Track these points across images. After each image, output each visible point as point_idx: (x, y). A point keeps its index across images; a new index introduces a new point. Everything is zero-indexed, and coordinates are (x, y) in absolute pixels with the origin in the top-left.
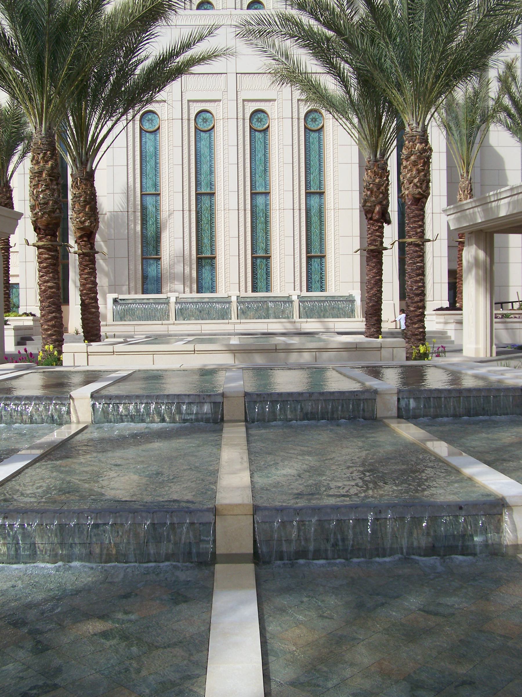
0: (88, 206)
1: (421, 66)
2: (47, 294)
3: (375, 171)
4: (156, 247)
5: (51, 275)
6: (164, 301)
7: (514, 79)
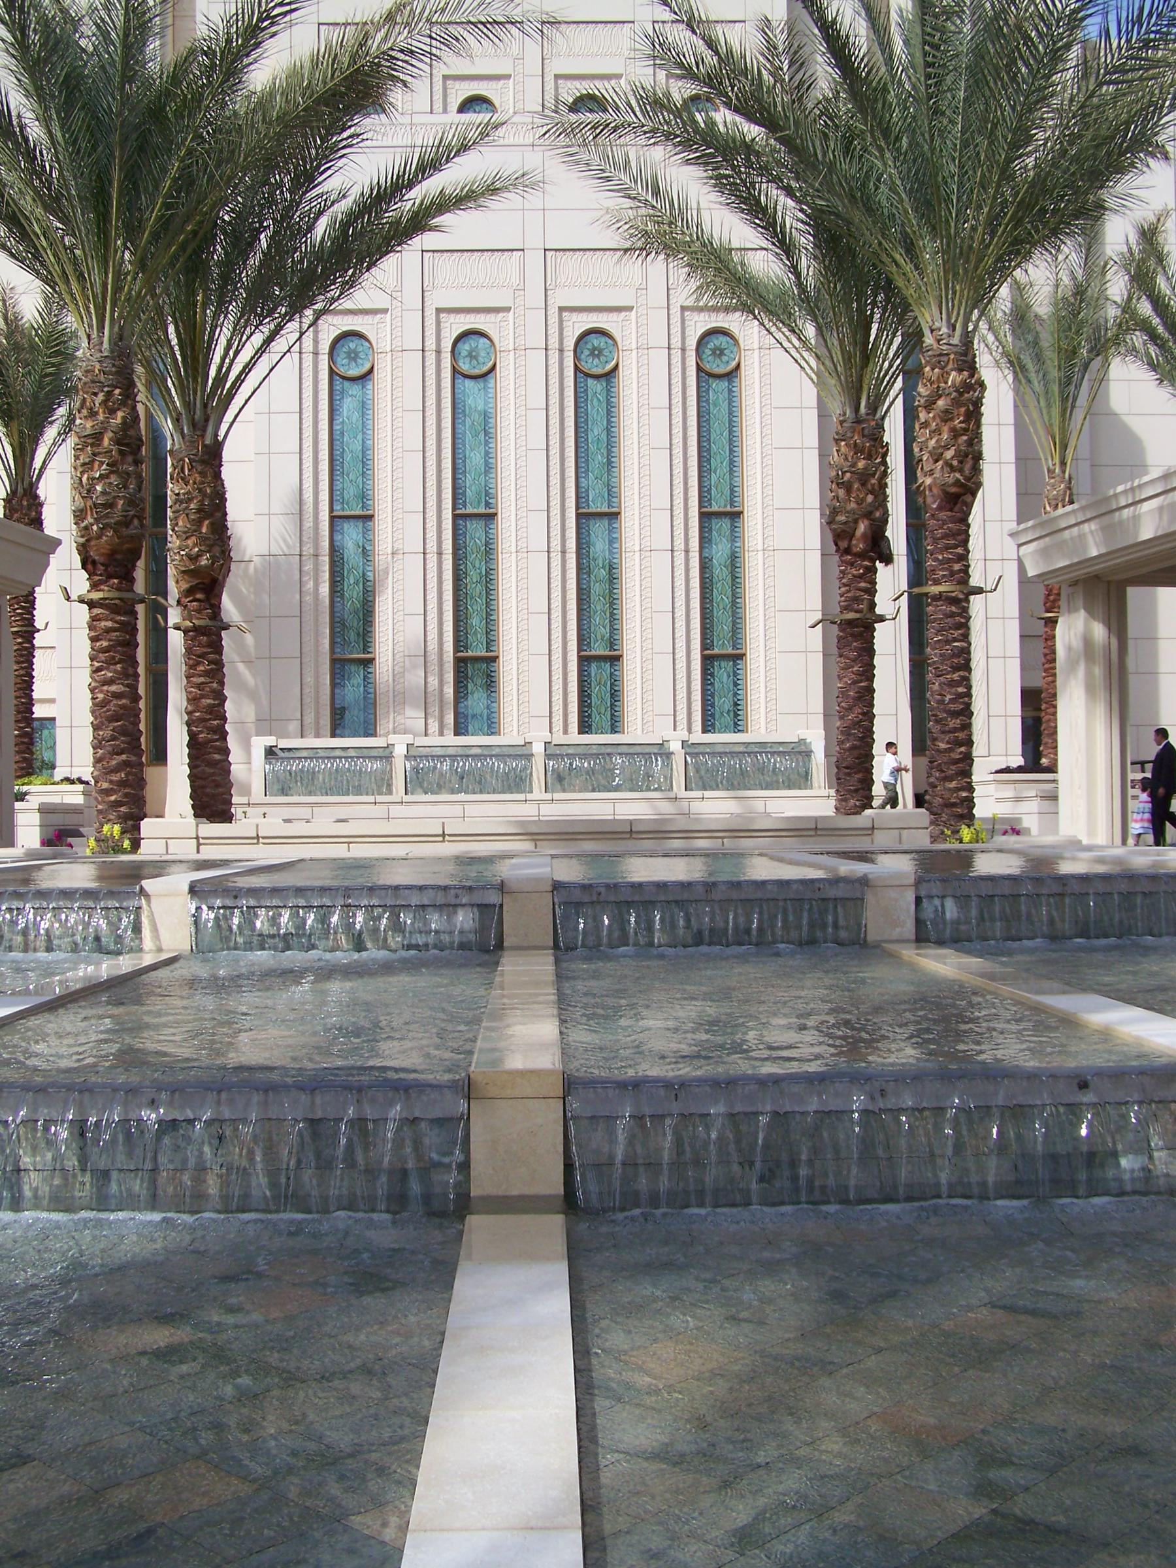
0: (207, 522)
1: (958, 201)
2: (108, 711)
3: (855, 444)
4: (364, 635)
5: (119, 667)
6: (380, 753)
7: (1161, 259)
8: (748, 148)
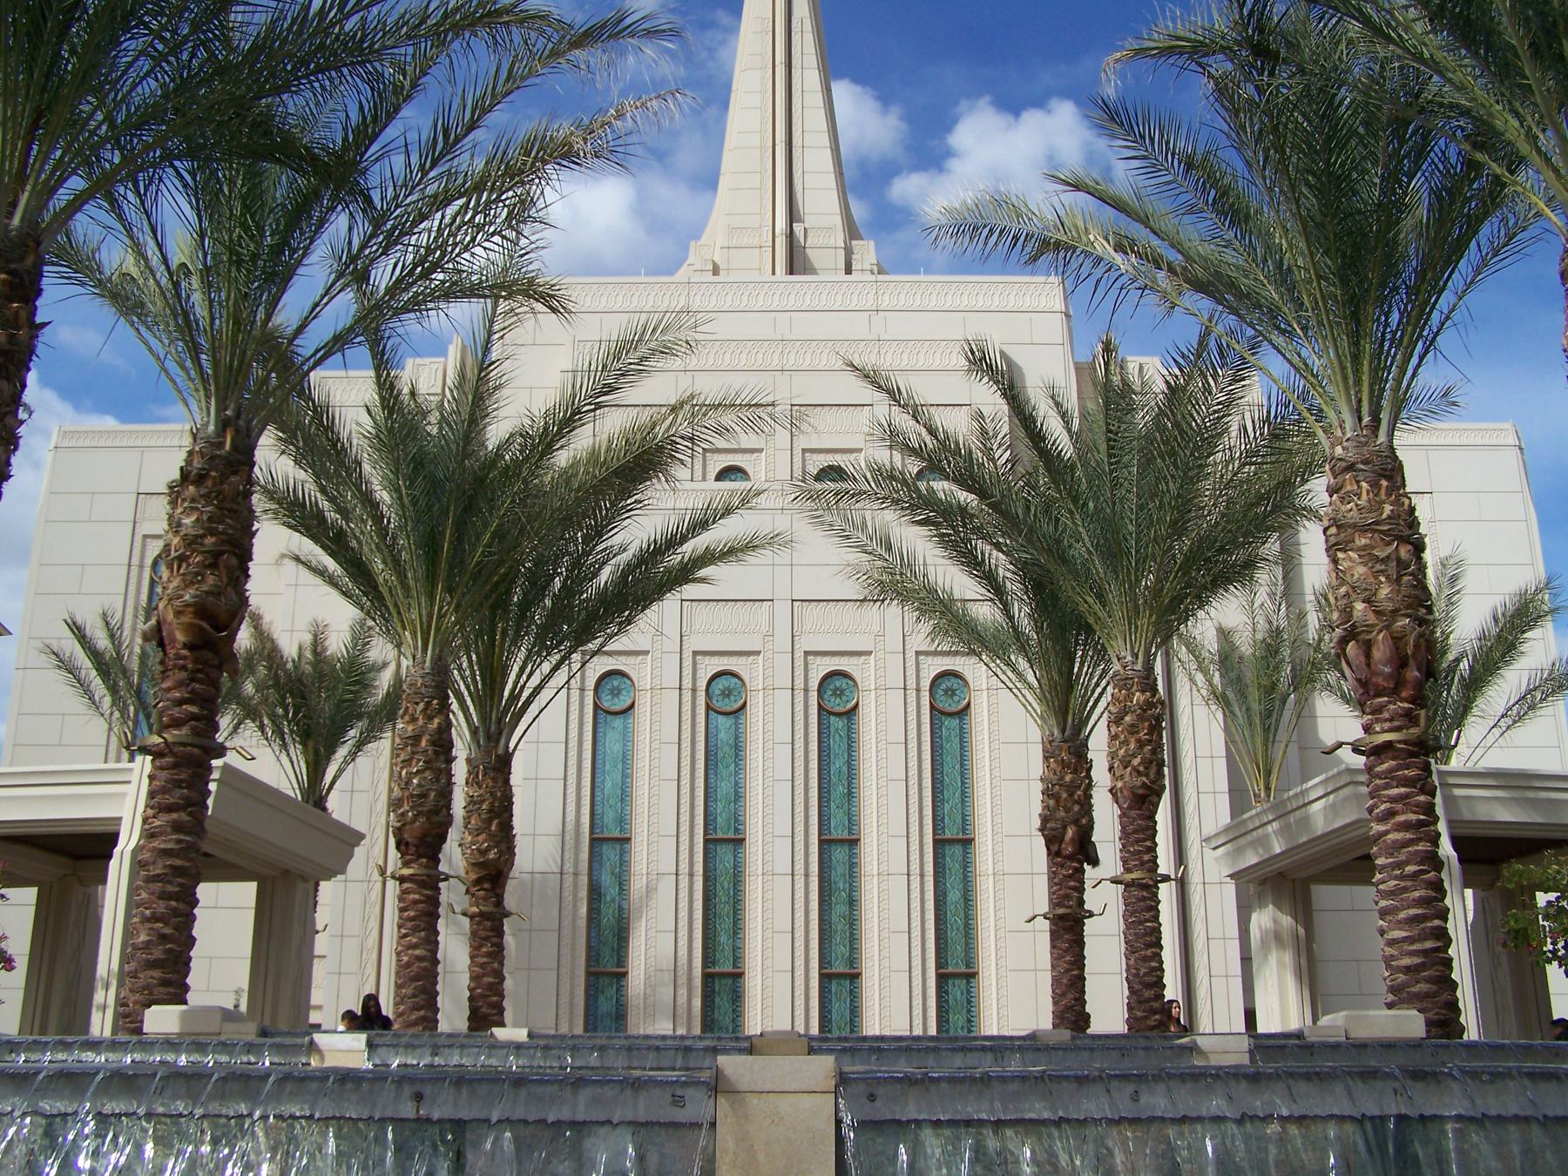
8: (963, 510)
